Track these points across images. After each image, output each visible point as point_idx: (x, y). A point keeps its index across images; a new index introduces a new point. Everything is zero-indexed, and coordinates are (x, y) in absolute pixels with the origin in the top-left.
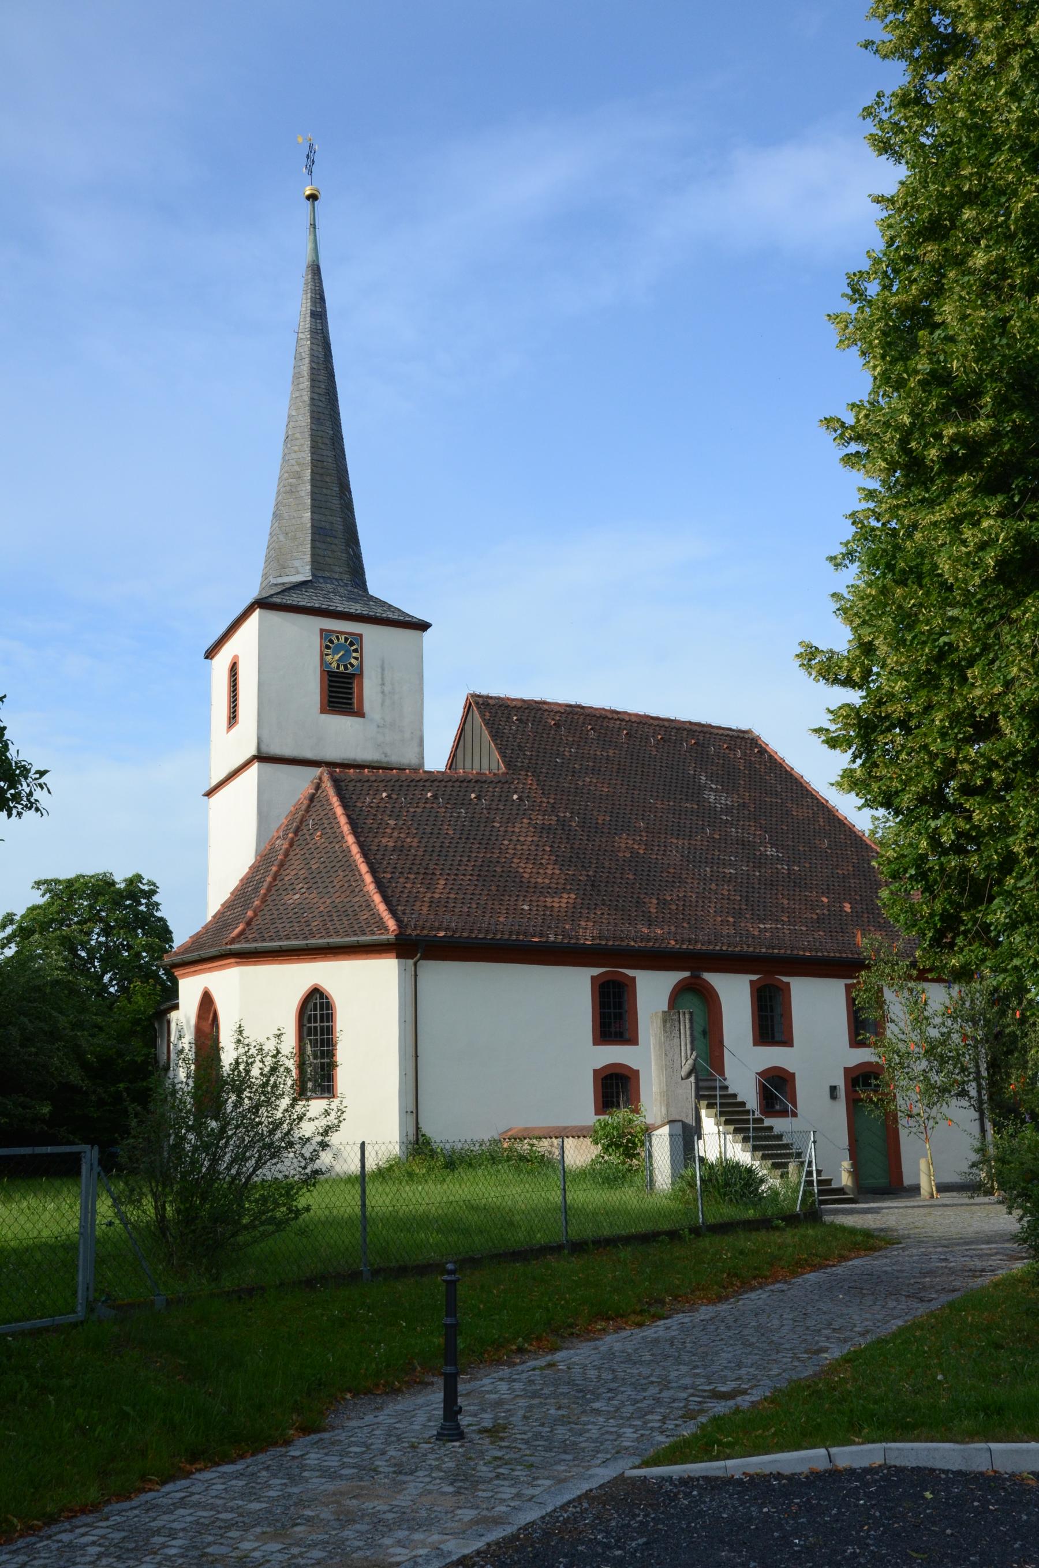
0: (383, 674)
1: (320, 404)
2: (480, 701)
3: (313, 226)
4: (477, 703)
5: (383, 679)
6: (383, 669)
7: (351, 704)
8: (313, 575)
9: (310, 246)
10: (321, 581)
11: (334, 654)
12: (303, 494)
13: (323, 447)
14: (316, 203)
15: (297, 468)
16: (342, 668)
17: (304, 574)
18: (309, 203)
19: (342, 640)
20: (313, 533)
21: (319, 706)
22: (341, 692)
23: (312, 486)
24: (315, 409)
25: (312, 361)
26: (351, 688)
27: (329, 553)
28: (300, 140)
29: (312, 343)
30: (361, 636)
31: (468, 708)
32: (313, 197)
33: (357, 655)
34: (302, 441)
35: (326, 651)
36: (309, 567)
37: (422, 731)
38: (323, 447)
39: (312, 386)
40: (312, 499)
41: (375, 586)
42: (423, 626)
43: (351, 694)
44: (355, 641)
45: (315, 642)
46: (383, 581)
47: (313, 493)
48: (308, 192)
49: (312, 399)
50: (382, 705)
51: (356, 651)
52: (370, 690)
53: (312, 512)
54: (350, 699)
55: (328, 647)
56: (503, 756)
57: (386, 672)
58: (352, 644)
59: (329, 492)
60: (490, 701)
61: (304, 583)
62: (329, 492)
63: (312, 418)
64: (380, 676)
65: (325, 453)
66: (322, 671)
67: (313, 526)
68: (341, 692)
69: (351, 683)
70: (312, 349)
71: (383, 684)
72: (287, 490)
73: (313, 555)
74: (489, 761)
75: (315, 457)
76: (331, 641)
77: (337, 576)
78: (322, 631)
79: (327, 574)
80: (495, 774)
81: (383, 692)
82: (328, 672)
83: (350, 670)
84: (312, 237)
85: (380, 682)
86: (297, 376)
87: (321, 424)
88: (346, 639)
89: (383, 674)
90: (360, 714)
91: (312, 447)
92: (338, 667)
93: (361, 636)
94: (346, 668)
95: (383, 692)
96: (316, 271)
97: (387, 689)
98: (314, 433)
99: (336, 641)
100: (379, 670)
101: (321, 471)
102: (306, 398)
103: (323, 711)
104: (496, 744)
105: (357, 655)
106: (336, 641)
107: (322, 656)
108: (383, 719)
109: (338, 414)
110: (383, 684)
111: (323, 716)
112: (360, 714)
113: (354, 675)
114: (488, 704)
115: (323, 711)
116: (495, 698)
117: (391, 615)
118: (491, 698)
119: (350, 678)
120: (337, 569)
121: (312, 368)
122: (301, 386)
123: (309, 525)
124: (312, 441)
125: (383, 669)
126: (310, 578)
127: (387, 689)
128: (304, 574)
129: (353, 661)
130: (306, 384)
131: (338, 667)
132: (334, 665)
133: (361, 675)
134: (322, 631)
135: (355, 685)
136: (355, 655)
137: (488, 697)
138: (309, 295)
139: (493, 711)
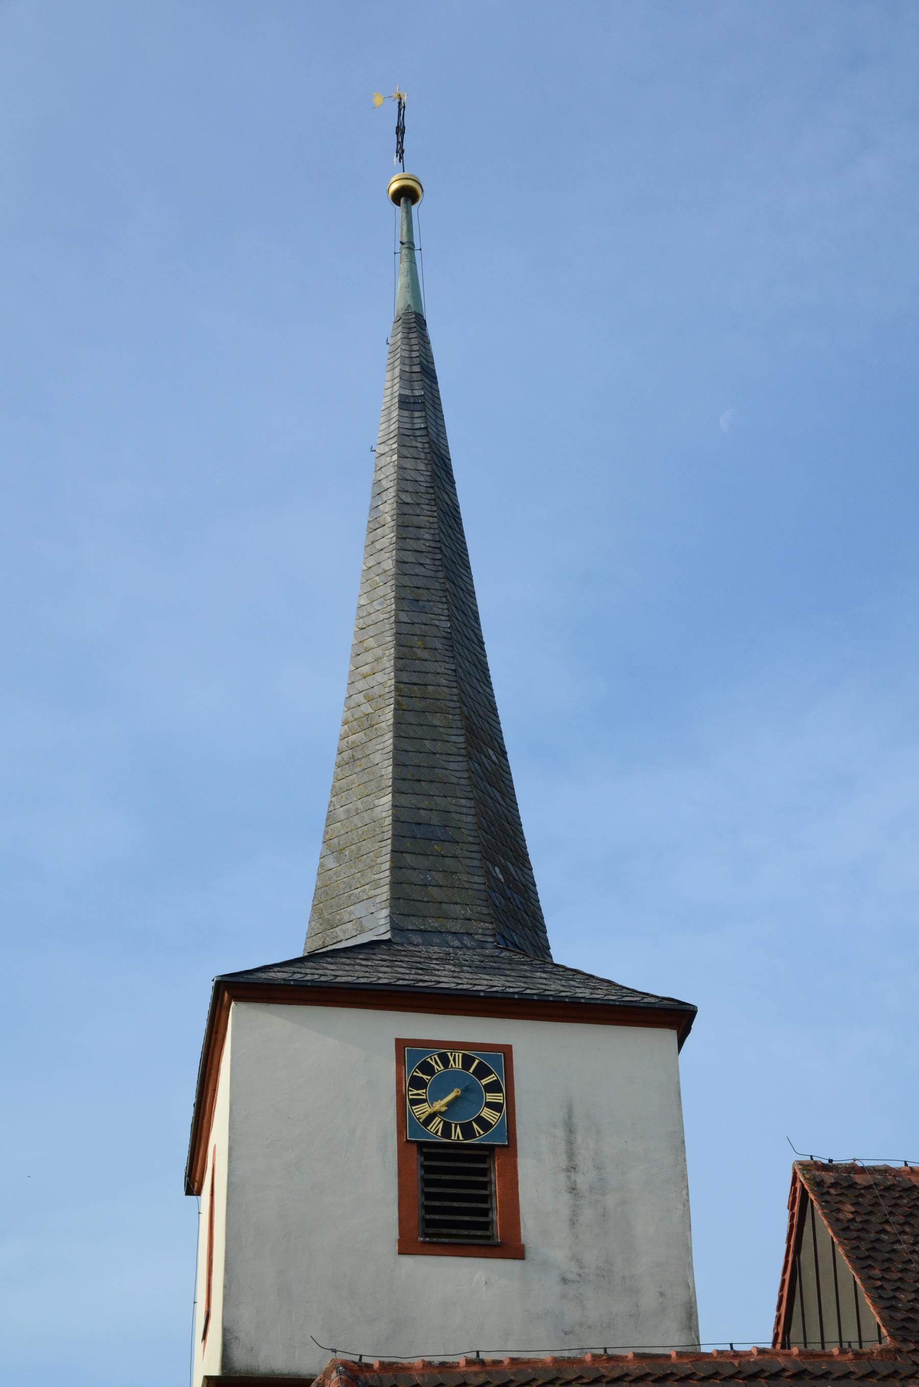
0: (570, 1143)
1: (419, 570)
2: (829, 1178)
3: (409, 245)
4: (819, 1184)
5: (571, 1154)
6: (570, 1129)
7: (486, 1226)
8: (395, 928)
9: (402, 281)
10: (417, 939)
11: (434, 1098)
12: (377, 758)
13: (425, 655)
14: (414, 208)
15: (367, 708)
16: (457, 1134)
17: (379, 926)
18: (400, 211)
19: (456, 1063)
20: (397, 837)
21: (395, 1234)
22: (456, 1195)
23: (397, 737)
24: (406, 581)
25: (400, 490)
26: (485, 1185)
27: (439, 877)
28: (378, 100)
29: (401, 457)
30: (507, 1050)
31: (800, 1206)
32: (407, 195)
33: (498, 1098)
34: (379, 652)
35: (413, 1093)
36: (385, 912)
37: (689, 1287)
38: (425, 655)
39: (400, 538)
40: (396, 765)
41: (565, 950)
42: (677, 1017)
43: (486, 1199)
44: (492, 1069)
45: (386, 1070)
46: (582, 940)
47: (398, 751)
48: (395, 186)
49: (400, 562)
50: (573, 1223)
51: (494, 1087)
52: (537, 1187)
53: (396, 792)
54: (485, 1212)
55: (417, 1083)
56: (887, 1306)
57: (579, 1138)
58: (482, 1071)
59: (439, 747)
60: (859, 1179)
61: (373, 945)
62: (439, 747)
63: (399, 599)
64: (563, 1147)
65: (431, 666)
66: (404, 1145)
67: (396, 820)
68: (456, 1195)
69: (485, 1172)
70: (401, 468)
71: (572, 1168)
72: (351, 758)
73: (395, 884)
74: (858, 1323)
75: (405, 677)
76: (427, 1068)
77: (457, 927)
78: (401, 1044)
79: (434, 924)
80: (858, 1355)
81: (573, 1189)
82: (421, 1145)
83: (480, 1137)
84: (404, 266)
85: (563, 1161)
86: (375, 525)
87: (423, 611)
88: (467, 1061)
89: (570, 1143)
90: (511, 1248)
91: (397, 658)
92: (447, 1131)
93: (507, 1050)
94: (467, 1131)
95: (573, 1189)
96: (414, 324)
97: (582, 1180)
98: (405, 629)
99: (439, 1068)
100: (560, 1133)
101: (418, 704)
102: (389, 565)
103: (407, 1246)
104: (867, 1279)
105: (498, 1098)
106: (439, 1068)
107: (403, 1105)
108: (577, 1260)
109: (472, 594)
110: (572, 1168)
111: (409, 1262)
112: (511, 1248)
113: (491, 1148)
114: (853, 1185)
115: (407, 1246)
116: (873, 1170)
117: (584, 993)
118: (863, 1170)
119: (483, 1159)
120: (458, 910)
121: (401, 503)
122: (378, 546)
123: (389, 820)
124: (399, 645)
125: (570, 1129)
126: (387, 936)
127: (582, 1180)
128: (379, 926)
129: (486, 1113)
130: (388, 536)
131: (447, 1131)
132: (437, 1125)
133: (510, 1148)
134: (401, 1044)
135: (495, 1176)
136: (490, 1097)
137: (853, 1169)
138: (397, 372)
139: (867, 1200)
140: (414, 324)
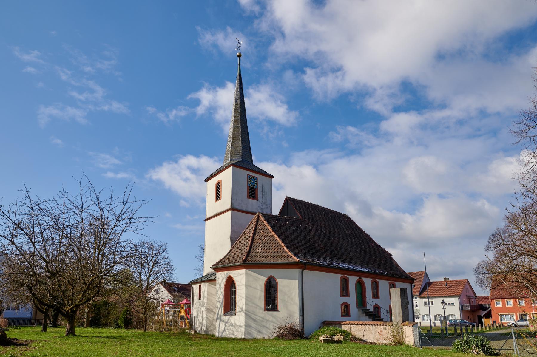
42: (272, 177)
44: (255, 179)
96: (240, 75)
112: (257, 200)
140: (240, 75)
